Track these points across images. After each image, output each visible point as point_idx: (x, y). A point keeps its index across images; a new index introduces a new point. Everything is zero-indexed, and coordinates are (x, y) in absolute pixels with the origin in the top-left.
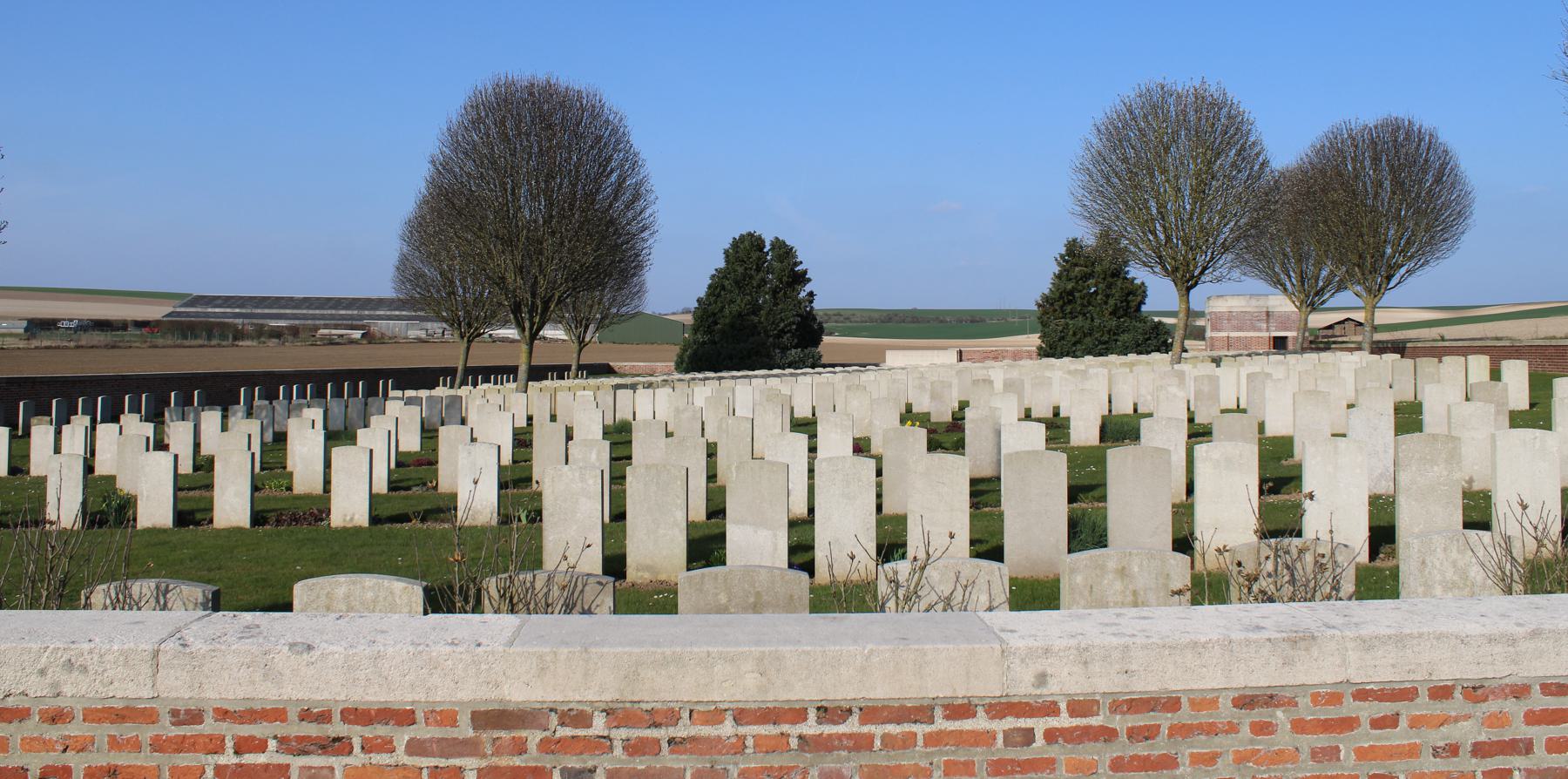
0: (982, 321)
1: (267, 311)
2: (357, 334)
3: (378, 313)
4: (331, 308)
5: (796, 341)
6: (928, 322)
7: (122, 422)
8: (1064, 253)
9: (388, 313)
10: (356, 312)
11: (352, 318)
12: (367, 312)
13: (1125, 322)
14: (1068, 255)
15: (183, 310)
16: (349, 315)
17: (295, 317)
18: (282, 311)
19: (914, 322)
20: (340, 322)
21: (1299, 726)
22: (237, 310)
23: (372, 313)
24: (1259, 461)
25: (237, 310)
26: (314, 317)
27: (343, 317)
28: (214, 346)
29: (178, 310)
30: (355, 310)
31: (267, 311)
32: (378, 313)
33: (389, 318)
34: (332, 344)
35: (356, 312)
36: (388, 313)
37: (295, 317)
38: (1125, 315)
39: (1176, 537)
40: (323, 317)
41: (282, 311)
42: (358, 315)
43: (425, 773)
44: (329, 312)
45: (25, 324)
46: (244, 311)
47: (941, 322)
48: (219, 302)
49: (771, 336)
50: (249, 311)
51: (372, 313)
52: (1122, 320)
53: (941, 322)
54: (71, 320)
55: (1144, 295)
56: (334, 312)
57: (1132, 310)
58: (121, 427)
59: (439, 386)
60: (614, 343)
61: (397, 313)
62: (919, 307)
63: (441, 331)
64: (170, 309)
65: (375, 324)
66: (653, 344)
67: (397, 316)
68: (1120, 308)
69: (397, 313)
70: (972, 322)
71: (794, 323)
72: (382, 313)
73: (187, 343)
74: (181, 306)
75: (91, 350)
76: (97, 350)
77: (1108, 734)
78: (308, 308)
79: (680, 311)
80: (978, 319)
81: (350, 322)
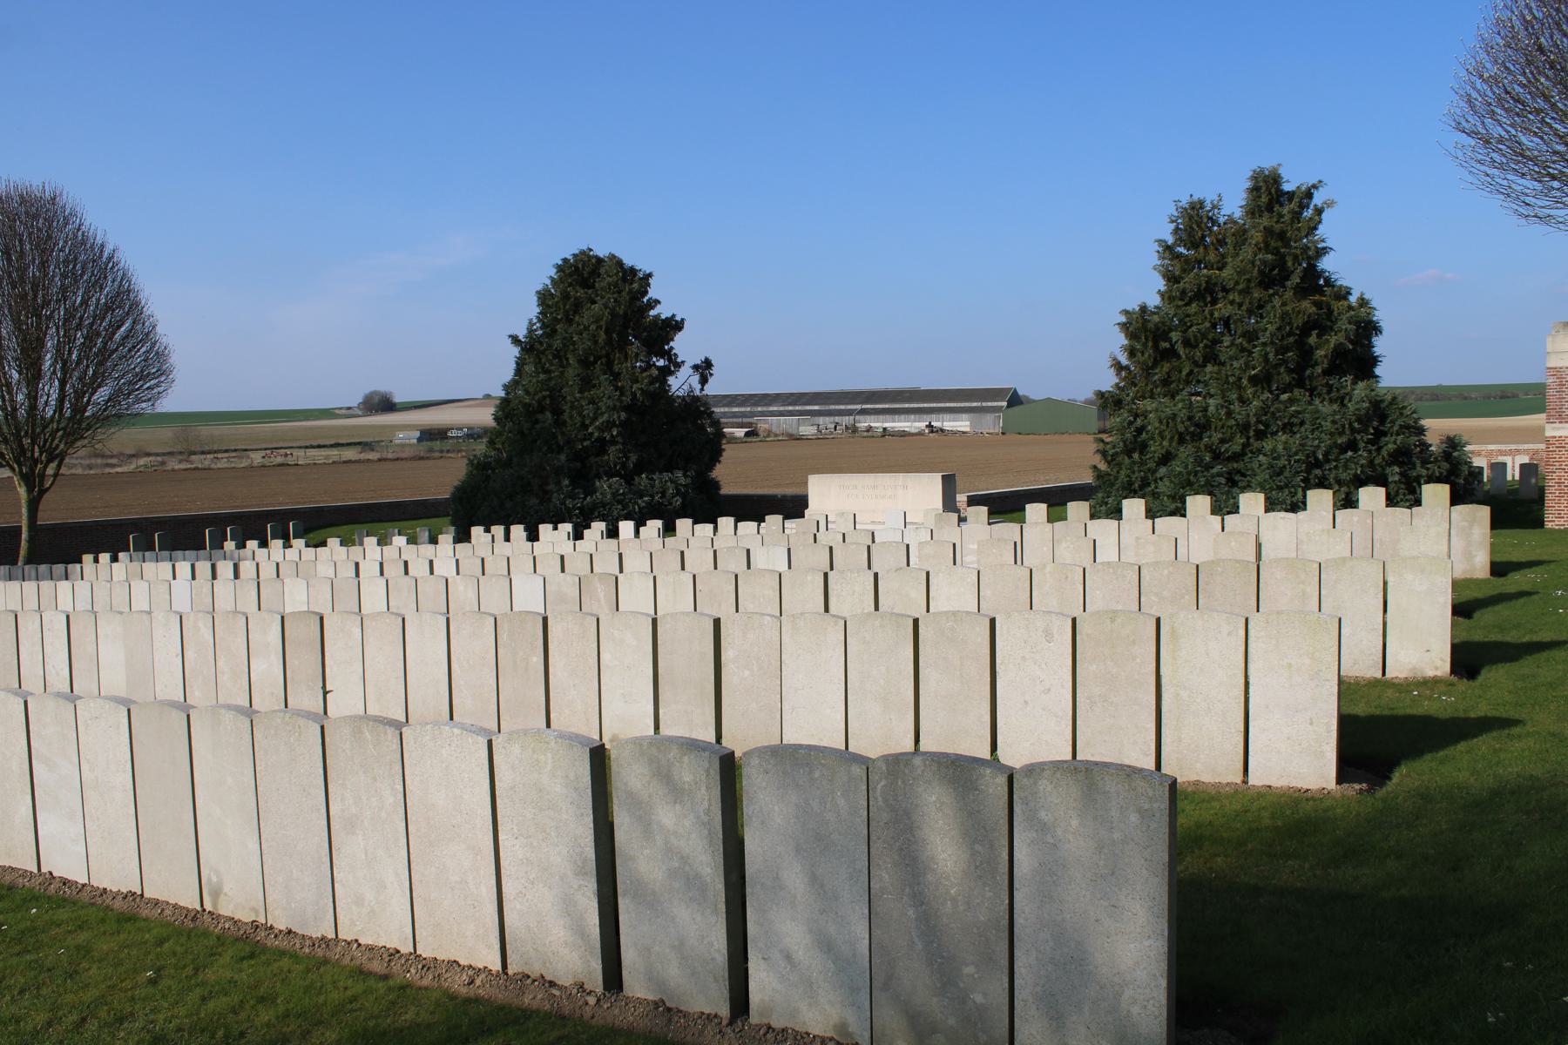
0: (1515, 396)
3: (771, 409)
4: (725, 406)
5: (633, 458)
6: (1450, 399)
7: (492, 532)
8: (1170, 240)
9: (782, 408)
10: (748, 409)
11: (743, 415)
12: (759, 409)
13: (1291, 401)
14: (1180, 241)
16: (741, 412)
19: (1433, 400)
23: (765, 409)
30: (748, 406)
32: (771, 409)
33: (781, 414)
35: (748, 409)
36: (782, 408)
38: (1300, 383)
39: (1456, 602)
42: (750, 412)
45: (418, 434)
47: (1465, 398)
51: (765, 409)
52: (1285, 397)
53: (1465, 398)
54: (461, 429)
56: (726, 409)
57: (1319, 370)
58: (493, 536)
59: (227, 540)
60: (1020, 434)
61: (790, 408)
62: (1446, 383)
66: (1063, 434)
67: (791, 411)
68: (1277, 366)
69: (790, 408)
70: (1502, 397)
71: (614, 424)
72: (775, 409)
75: (396, 462)
76: (402, 462)
79: (355, 400)
80: (1509, 395)
81: (740, 420)
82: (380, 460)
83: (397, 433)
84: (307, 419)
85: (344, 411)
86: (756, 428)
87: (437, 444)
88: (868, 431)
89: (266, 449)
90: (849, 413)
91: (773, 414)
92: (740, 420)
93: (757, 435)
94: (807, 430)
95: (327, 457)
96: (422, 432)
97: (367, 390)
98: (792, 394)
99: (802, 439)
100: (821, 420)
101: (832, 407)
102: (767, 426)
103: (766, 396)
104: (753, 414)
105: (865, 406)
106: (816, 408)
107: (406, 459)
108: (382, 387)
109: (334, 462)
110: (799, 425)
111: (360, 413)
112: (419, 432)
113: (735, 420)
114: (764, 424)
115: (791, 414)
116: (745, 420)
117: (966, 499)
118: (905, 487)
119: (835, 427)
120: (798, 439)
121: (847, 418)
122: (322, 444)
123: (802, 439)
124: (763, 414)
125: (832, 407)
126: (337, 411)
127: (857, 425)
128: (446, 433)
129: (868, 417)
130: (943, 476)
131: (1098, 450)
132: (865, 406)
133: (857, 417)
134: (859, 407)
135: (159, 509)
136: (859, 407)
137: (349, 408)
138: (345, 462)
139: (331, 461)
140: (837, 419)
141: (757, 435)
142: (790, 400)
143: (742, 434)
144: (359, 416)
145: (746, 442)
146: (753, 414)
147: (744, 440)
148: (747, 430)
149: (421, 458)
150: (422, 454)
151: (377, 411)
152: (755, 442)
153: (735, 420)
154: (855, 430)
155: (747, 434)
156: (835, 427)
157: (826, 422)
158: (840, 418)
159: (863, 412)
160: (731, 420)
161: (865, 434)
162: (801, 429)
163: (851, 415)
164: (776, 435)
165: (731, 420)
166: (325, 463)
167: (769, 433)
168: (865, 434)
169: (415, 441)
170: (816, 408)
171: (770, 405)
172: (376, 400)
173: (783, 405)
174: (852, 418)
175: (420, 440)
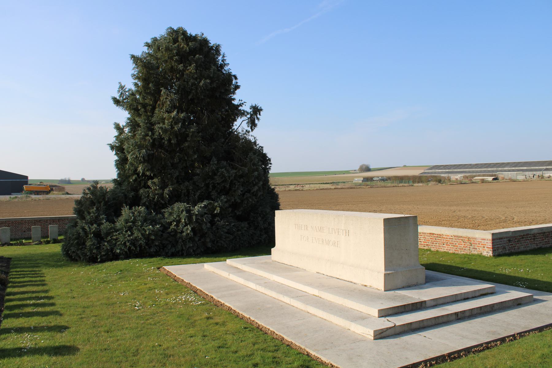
1: (459, 170)
2: (490, 179)
10: (495, 169)
11: (493, 171)
15: (427, 171)
17: (469, 172)
18: (465, 170)
20: (484, 174)
21: (487, 247)
22: (447, 170)
23: (502, 169)
24: (384, 245)
25: (447, 170)
26: (473, 172)
27: (489, 171)
28: (400, 186)
29: (426, 171)
31: (459, 170)
33: (509, 171)
34: (461, 183)
35: (495, 169)
36: (510, 169)
37: (469, 172)
40: (477, 172)
41: (465, 170)
43: (3, 276)
44: (484, 169)
45: (362, 179)
46: (450, 170)
48: (442, 167)
49: (144, 205)
50: (452, 170)
51: (502, 169)
55: (116, 160)
61: (513, 168)
63: (532, 176)
64: (422, 171)
65: (502, 174)
69: (513, 168)
73: (401, 185)
74: (427, 170)
77: (482, 244)
78: (476, 168)
81: (491, 173)
82: (335, 189)
83: (355, 178)
84: (339, 174)
85: (353, 172)
86: (498, 176)
87: (369, 183)
88: (549, 178)
89: (295, 184)
90: (540, 170)
91: (505, 171)
92: (491, 173)
93: (498, 179)
94: (521, 177)
95: (315, 187)
96: (364, 178)
97: (361, 164)
98: (515, 163)
99: (516, 181)
100: (527, 173)
101: (532, 168)
102: (502, 176)
103: (503, 164)
104: (497, 171)
105: (548, 167)
106: (525, 168)
107: (345, 188)
108: (366, 163)
109: (317, 189)
110: (517, 175)
111: (358, 172)
112: (363, 178)
113: (489, 173)
114: (501, 175)
115: (513, 171)
116: (493, 173)
117: (490, 237)
118: (347, 233)
119: (534, 176)
120: (515, 181)
121: (539, 172)
122: (327, 182)
123: (516, 181)
124: (501, 171)
125: (532, 168)
126: (351, 171)
127: (544, 175)
128: (373, 178)
129: (549, 172)
130: (387, 221)
131: (110, 144)
132: (548, 167)
133: (544, 172)
134: (545, 167)
135: (35, 215)
136: (545, 167)
137: (355, 170)
138: (321, 189)
139: (316, 189)
140: (534, 173)
141: (498, 179)
142: (513, 165)
143: (491, 179)
144: (357, 173)
145: (493, 182)
146: (497, 171)
147: (492, 181)
148: (493, 177)
149: (352, 188)
150: (352, 187)
151: (364, 171)
152: (494, 182)
153: (489, 173)
154: (543, 177)
155: (494, 179)
156: (534, 176)
157: (530, 174)
158: (536, 172)
159: (547, 170)
160: (487, 173)
161: (547, 179)
162: (518, 177)
163: (541, 171)
164: (506, 180)
165: (487, 173)
166: (313, 190)
167: (503, 178)
168: (547, 179)
169: (361, 182)
170: (525, 168)
171: (504, 167)
172: (364, 167)
173: (510, 167)
174: (541, 172)
175: (363, 181)
